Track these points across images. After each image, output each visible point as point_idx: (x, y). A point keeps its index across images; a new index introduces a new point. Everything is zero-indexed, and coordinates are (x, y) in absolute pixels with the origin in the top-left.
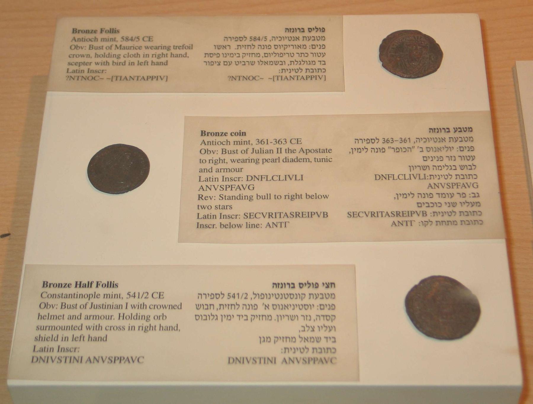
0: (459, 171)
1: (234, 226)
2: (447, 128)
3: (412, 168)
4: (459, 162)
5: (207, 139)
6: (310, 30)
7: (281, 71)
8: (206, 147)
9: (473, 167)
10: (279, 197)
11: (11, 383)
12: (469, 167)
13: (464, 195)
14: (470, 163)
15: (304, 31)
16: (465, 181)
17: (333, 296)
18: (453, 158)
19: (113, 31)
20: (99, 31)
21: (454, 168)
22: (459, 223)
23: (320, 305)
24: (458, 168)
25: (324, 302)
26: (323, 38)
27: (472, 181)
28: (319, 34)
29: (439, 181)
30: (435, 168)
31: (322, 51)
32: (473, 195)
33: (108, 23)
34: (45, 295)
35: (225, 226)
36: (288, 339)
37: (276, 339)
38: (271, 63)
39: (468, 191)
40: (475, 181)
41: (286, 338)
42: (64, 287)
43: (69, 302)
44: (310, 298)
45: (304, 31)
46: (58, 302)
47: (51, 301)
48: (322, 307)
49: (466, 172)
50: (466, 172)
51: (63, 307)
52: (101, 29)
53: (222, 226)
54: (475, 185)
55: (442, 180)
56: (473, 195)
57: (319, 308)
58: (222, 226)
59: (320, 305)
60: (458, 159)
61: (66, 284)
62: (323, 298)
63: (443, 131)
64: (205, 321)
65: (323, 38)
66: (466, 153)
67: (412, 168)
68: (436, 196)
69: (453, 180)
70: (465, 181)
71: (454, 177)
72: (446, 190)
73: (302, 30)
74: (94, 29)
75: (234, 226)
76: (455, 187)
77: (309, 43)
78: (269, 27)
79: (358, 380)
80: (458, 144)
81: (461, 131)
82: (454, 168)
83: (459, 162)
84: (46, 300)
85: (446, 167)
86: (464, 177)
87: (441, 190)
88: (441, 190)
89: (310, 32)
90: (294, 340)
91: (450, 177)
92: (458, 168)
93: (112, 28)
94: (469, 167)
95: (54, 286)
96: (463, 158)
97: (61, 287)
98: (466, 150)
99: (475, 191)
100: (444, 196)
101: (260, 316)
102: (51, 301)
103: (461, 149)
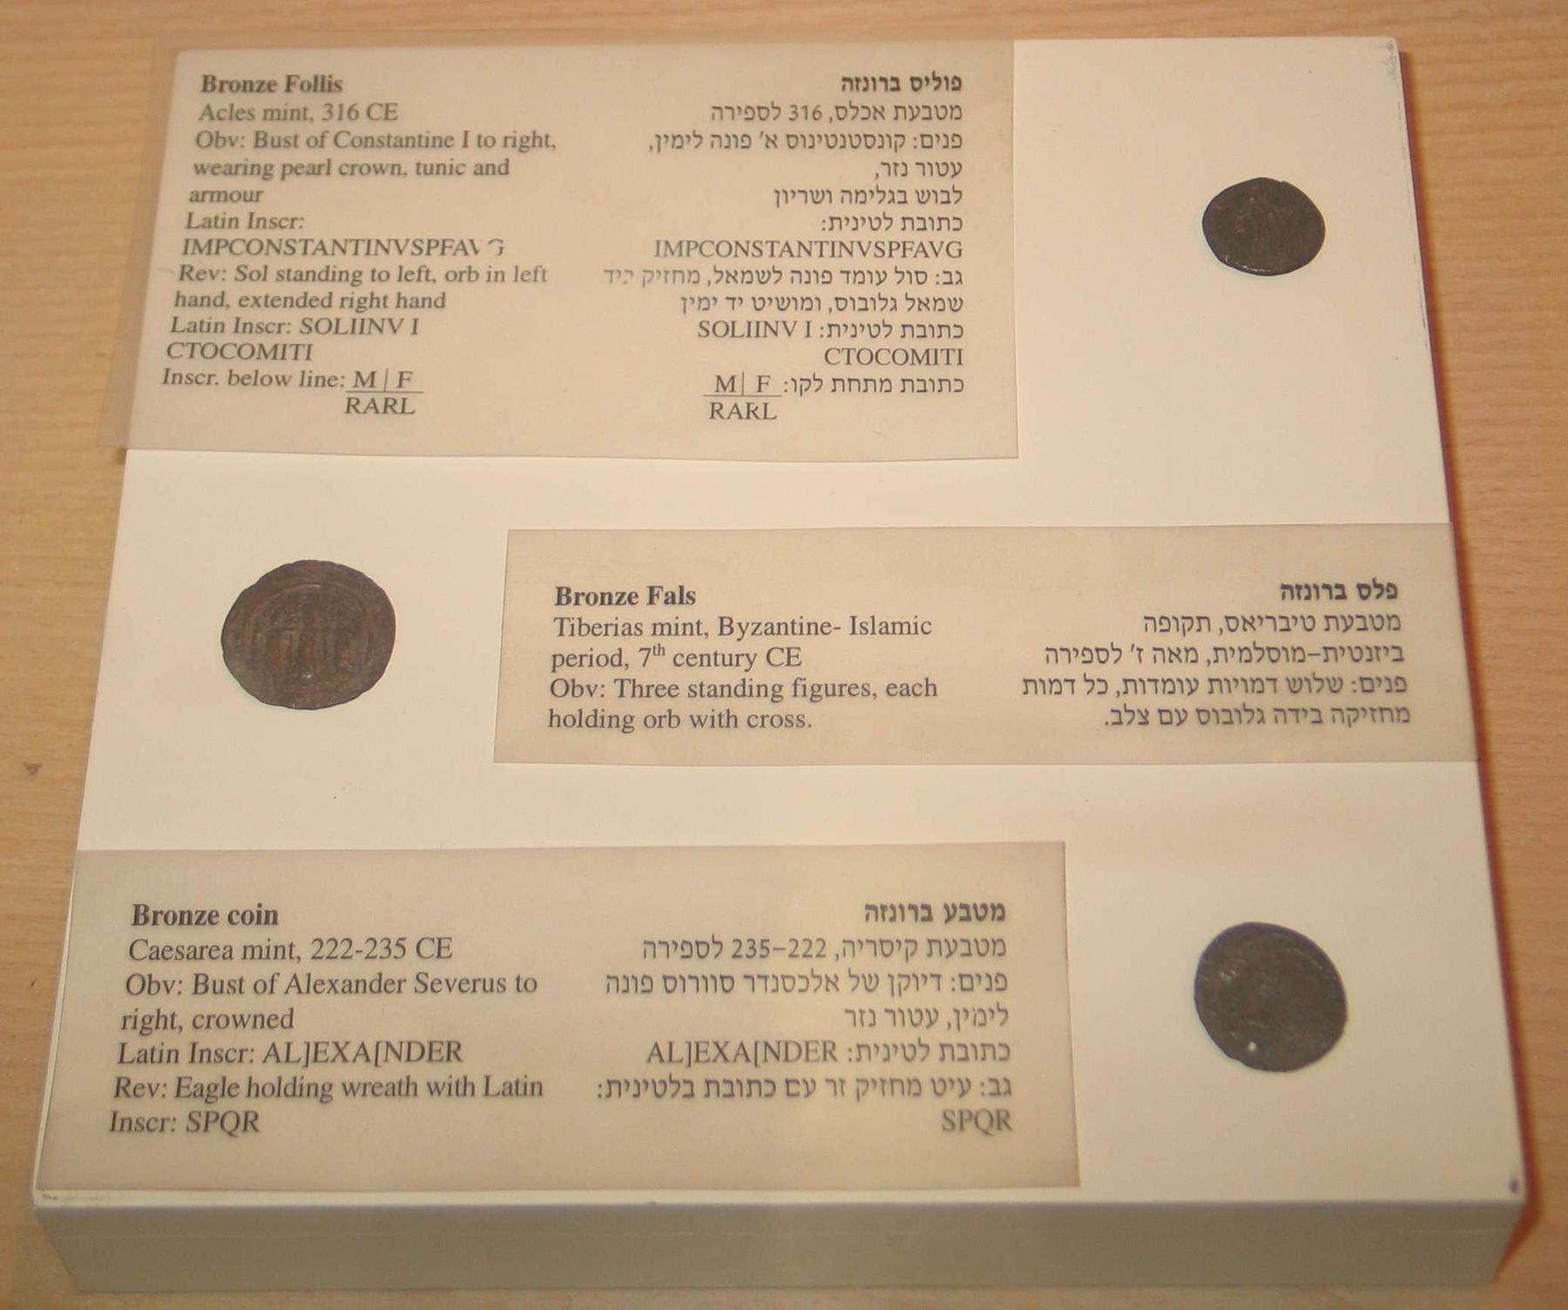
0: (913, 209)
1: (266, 381)
2: (893, 79)
3: (782, 196)
4: (915, 181)
5: (219, 101)
6: (917, 84)
7: (828, 225)
8: (214, 127)
9: (954, 197)
10: (384, 276)
11: (40, 1200)
12: (943, 197)
13: (920, 277)
14: (946, 183)
15: (897, 89)
16: (925, 237)
17: (999, 948)
18: (901, 170)
19: (324, 84)
20: (282, 83)
21: (899, 197)
22: (897, 386)
23: (961, 976)
24: (911, 197)
25: (973, 965)
26: (955, 112)
27: (946, 235)
28: (946, 97)
29: (855, 237)
30: (847, 196)
31: (951, 156)
32: (946, 278)
33: (307, 64)
34: (141, 950)
35: (241, 380)
36: (897, 1087)
37: (862, 1087)
38: (939, 305)
39: (935, 266)
40: (955, 236)
41: (892, 1081)
42: (197, 923)
43: (217, 970)
44: (930, 955)
45: (897, 89)
46: (183, 972)
47: (161, 970)
48: (967, 983)
49: (932, 210)
50: (932, 210)
51: (201, 989)
52: (289, 78)
53: (234, 380)
54: (953, 250)
55: (865, 234)
56: (946, 278)
57: (957, 985)
58: (234, 380)
59: (961, 976)
60: (915, 172)
61: (203, 913)
62: (969, 954)
63: (881, 86)
64: (728, 1101)
65: (955, 112)
66: (937, 155)
67: (782, 196)
68: (839, 279)
69: (895, 234)
70: (925, 237)
71: (898, 223)
72: (870, 263)
73: (894, 85)
74: (267, 79)
75: (266, 381)
76: (898, 253)
77: (912, 130)
78: (806, 73)
79: (1075, 1182)
80: (920, 126)
81: (967, 919)
82: (899, 197)
83: (915, 181)
84: (146, 968)
85: (878, 196)
86: (924, 224)
87: (856, 262)
88: (856, 262)
89: (915, 89)
90: (915, 1088)
91: (884, 331)
92: (911, 197)
93: (320, 73)
94: (943, 197)
95: (166, 920)
96: (927, 168)
97: (189, 923)
98: (938, 147)
99: (953, 266)
100: (859, 278)
101: (883, 1081)
102: (161, 970)
103: (926, 141)
